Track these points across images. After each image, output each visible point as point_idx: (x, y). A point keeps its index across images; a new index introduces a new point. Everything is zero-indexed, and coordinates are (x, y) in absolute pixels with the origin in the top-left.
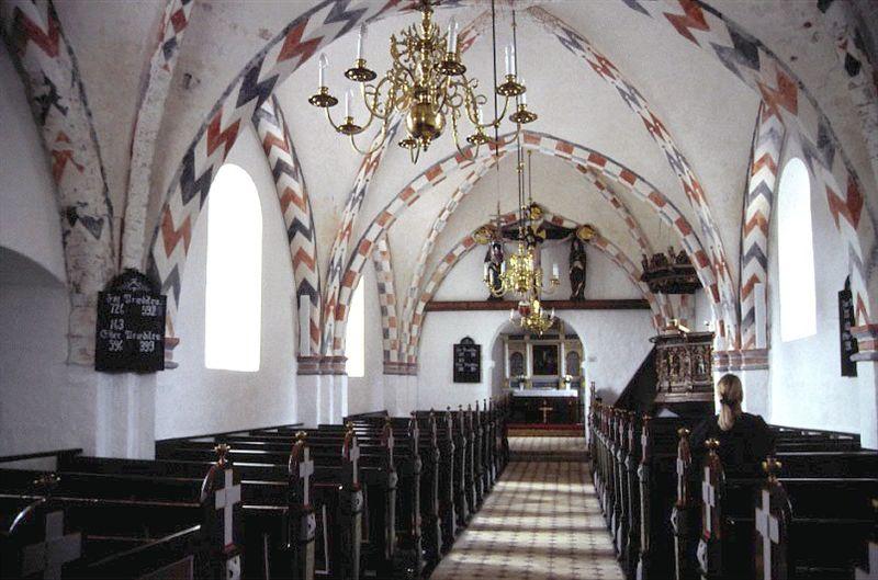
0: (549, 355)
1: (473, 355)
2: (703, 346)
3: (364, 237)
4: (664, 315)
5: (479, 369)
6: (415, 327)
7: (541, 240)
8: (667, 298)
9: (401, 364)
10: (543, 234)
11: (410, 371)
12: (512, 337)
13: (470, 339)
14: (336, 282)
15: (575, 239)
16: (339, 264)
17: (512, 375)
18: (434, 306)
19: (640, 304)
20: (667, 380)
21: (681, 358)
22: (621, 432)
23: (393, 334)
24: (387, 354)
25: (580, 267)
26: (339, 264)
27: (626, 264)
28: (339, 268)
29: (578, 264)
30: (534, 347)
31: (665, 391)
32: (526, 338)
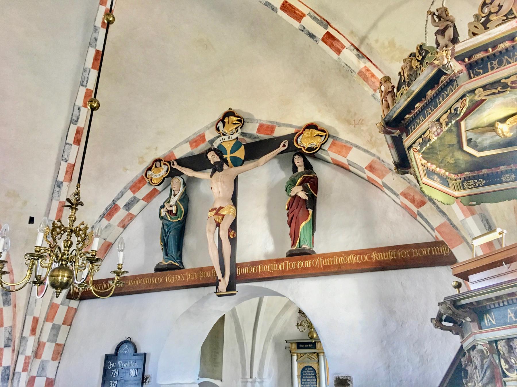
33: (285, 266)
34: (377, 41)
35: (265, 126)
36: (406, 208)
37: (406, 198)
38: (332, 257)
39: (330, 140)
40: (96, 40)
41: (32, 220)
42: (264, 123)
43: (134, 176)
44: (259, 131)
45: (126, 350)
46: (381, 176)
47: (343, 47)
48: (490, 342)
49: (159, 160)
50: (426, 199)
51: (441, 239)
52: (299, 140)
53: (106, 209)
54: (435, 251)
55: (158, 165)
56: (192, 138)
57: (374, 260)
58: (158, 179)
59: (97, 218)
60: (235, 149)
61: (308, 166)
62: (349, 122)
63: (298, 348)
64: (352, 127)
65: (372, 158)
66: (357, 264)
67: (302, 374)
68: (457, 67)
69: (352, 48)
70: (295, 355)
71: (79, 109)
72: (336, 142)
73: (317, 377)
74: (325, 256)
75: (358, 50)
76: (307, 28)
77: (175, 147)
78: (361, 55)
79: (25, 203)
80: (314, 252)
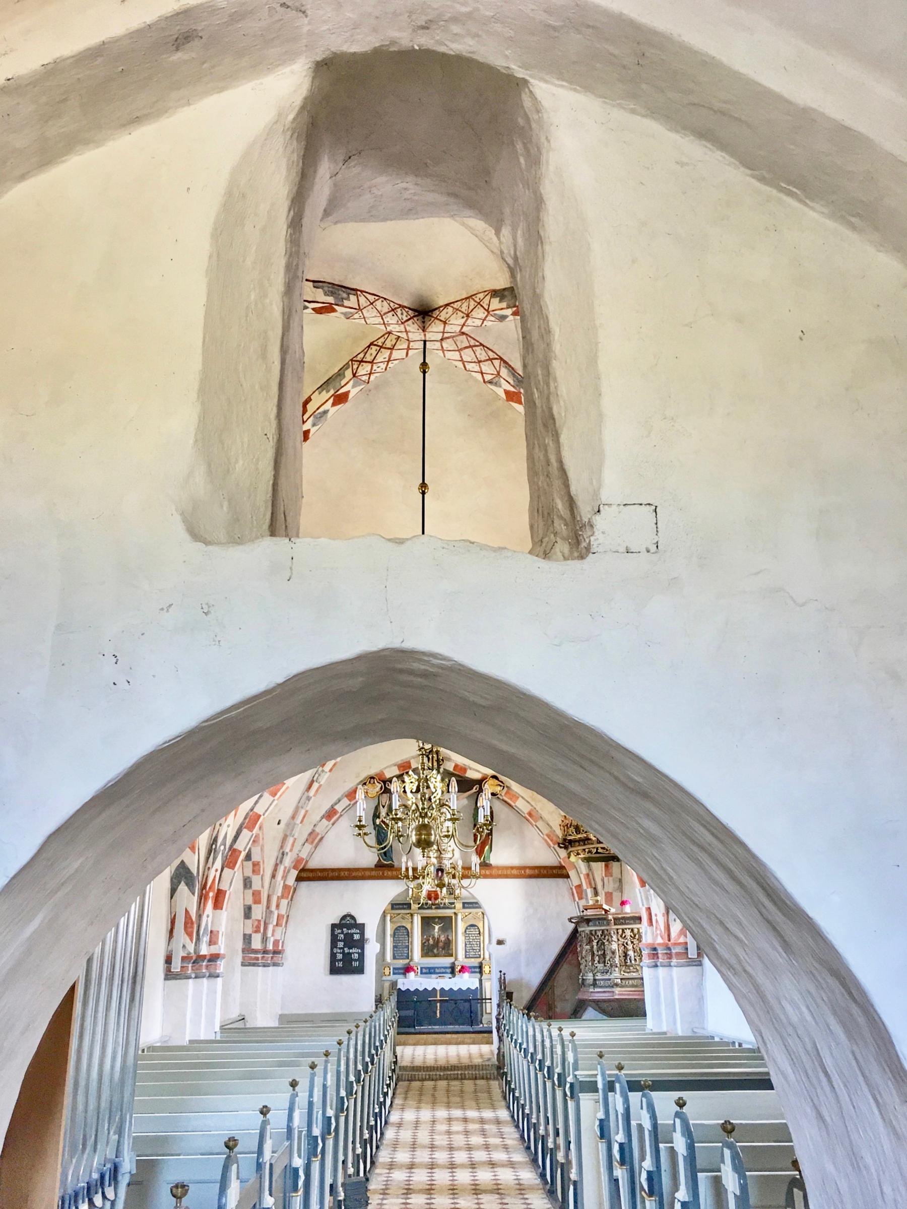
1: (357, 937)
2: (632, 930)
3: (252, 810)
4: (585, 886)
6: (284, 902)
8: (589, 866)
9: (265, 952)
13: (353, 918)
14: (218, 864)
16: (224, 844)
17: (394, 958)
18: (307, 875)
19: (558, 872)
20: (592, 971)
22: (515, 1022)
23: (258, 912)
24: (247, 939)
26: (224, 844)
28: (222, 848)
35: (459, 767)
36: (546, 841)
38: (503, 869)
39: (506, 789)
42: (459, 764)
44: (454, 769)
46: (535, 822)
49: (372, 778)
55: (372, 782)
56: (400, 762)
58: (372, 794)
59: (318, 818)
65: (531, 807)
70: (389, 915)
72: (510, 791)
73: (410, 935)
74: (498, 868)
77: (385, 768)
80: (491, 865)
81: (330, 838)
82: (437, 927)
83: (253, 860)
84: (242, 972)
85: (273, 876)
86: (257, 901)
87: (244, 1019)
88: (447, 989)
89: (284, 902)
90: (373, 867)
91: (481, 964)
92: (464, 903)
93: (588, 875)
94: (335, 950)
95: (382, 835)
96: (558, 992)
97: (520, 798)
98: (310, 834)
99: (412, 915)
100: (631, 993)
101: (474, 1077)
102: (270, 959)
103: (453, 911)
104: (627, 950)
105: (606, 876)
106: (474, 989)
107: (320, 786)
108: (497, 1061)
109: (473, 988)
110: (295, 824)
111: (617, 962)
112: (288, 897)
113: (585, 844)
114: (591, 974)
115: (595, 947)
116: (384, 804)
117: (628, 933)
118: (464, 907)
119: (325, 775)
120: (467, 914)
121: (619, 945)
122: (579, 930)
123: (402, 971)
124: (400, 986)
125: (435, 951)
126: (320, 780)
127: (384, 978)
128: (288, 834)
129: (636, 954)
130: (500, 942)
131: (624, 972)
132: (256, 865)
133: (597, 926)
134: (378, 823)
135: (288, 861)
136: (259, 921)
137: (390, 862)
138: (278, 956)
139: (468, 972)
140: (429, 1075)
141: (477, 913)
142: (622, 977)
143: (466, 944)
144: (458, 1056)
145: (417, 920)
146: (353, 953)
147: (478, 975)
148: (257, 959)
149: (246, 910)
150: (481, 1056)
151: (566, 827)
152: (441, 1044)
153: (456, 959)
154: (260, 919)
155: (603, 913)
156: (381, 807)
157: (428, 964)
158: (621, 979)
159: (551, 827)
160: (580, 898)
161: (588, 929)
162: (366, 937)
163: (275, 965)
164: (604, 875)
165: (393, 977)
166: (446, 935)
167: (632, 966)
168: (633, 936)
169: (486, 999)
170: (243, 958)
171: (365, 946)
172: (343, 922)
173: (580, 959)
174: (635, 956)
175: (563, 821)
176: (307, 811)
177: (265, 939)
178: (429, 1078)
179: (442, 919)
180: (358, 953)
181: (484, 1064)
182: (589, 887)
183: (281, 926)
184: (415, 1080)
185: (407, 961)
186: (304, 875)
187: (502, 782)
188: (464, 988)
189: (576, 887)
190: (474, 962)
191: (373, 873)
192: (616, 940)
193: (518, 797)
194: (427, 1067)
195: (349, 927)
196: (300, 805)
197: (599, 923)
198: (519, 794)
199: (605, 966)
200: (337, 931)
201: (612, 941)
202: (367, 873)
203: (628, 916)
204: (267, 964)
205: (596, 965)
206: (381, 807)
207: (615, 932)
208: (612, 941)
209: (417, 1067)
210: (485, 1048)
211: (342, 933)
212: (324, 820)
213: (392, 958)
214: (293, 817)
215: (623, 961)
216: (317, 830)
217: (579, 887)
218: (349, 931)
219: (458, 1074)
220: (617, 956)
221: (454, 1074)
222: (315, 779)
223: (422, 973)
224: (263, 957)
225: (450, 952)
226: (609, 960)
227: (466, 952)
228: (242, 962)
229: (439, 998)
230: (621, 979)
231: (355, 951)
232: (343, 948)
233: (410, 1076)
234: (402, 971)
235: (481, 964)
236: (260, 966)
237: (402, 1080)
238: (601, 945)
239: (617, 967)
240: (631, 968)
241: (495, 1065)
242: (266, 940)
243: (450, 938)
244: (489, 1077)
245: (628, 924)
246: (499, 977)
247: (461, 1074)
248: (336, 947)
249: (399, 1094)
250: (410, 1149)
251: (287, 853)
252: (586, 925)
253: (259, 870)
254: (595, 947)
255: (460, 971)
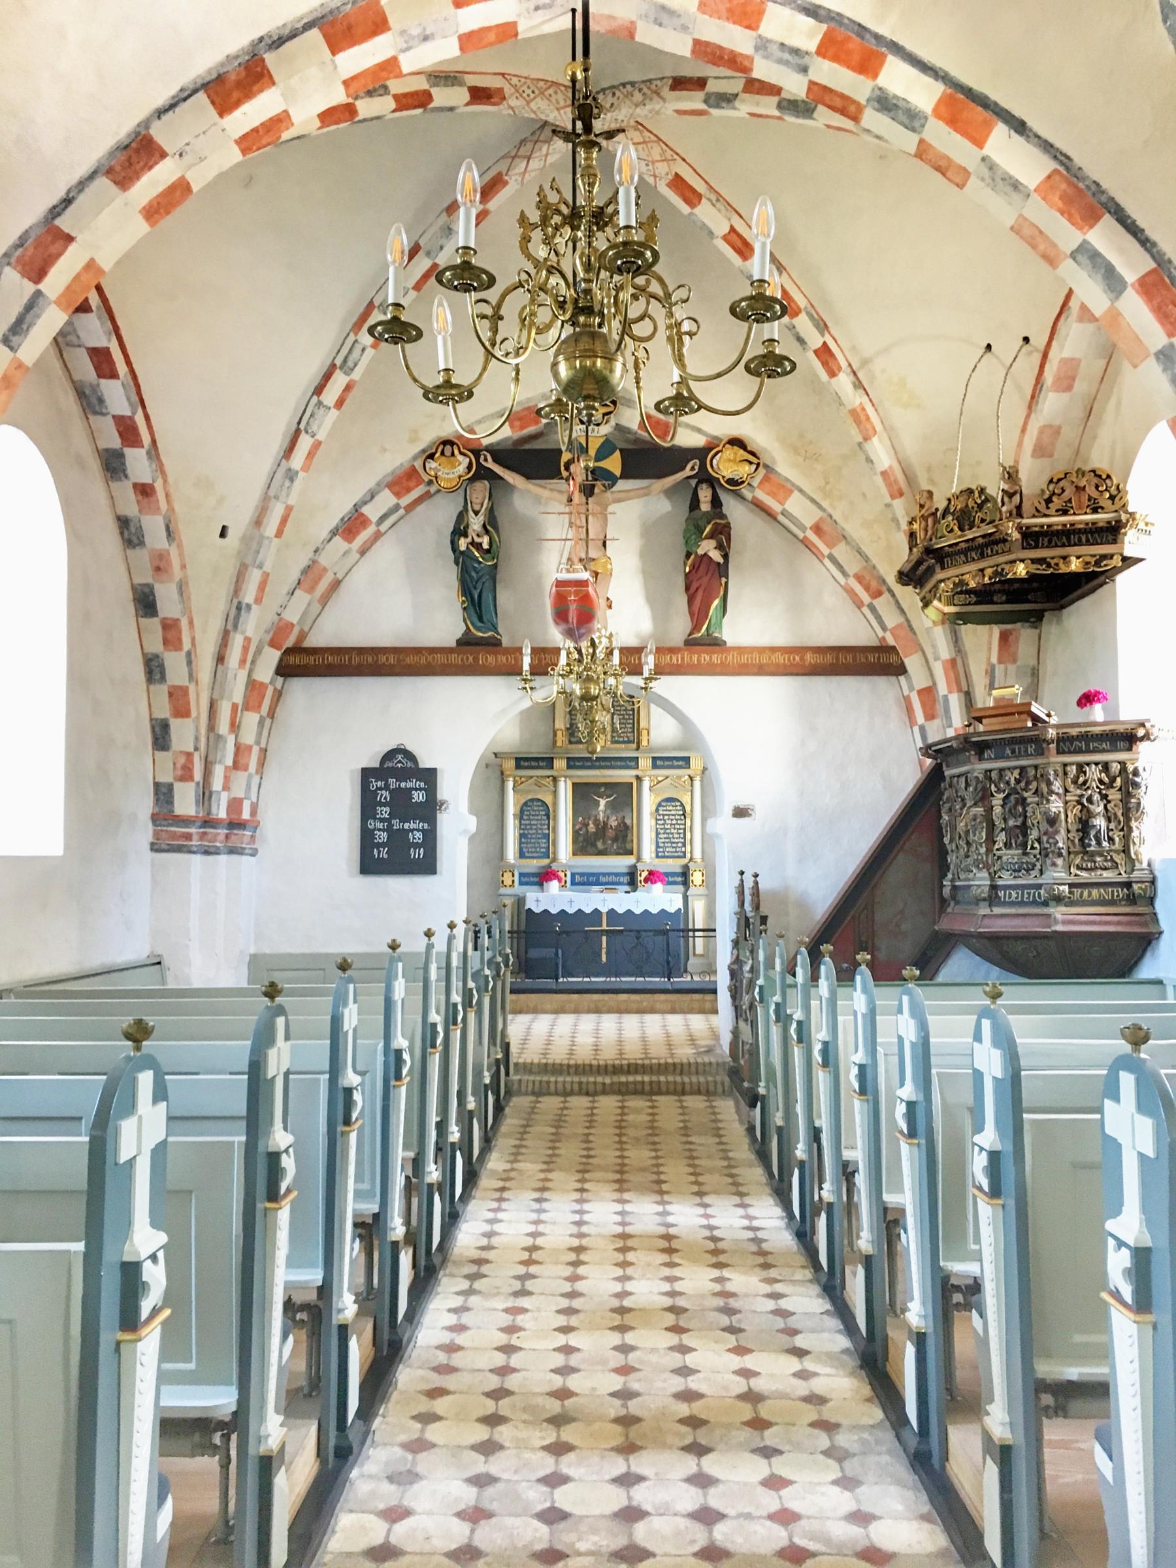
0: (613, 807)
1: (418, 797)
2: (1106, 767)
4: (942, 688)
5: (430, 839)
6: (250, 720)
7: (609, 479)
9: (209, 822)
10: (614, 464)
11: (234, 842)
12: (521, 762)
15: (706, 478)
17: (522, 855)
20: (987, 866)
21: (1031, 799)
23: (183, 734)
24: (163, 793)
25: (716, 556)
27: (841, 551)
29: (708, 547)
30: (575, 786)
31: (978, 901)
32: (560, 764)
33: (683, 658)
34: (883, 371)
37: (860, 582)
38: (752, 653)
39: (762, 472)
40: (442, 248)
41: (223, 533)
43: (397, 464)
44: (642, 425)
45: (400, 762)
46: (830, 545)
47: (840, 369)
48: (986, 771)
50: (884, 588)
51: (891, 641)
52: (715, 462)
53: (342, 519)
54: (884, 659)
57: (807, 663)
58: (449, 480)
59: (324, 534)
60: (603, 453)
61: (716, 502)
62: (795, 450)
63: (518, 766)
64: (801, 459)
66: (784, 665)
67: (522, 811)
68: (1016, 535)
69: (849, 370)
71: (363, 350)
72: (772, 476)
74: (741, 650)
75: (854, 373)
76: (798, 329)
78: (858, 385)
79: (221, 500)
81: (359, 580)
82: (603, 802)
83: (161, 614)
84: (153, 866)
85: (220, 659)
86: (182, 711)
87: (159, 963)
88: (621, 911)
89: (250, 720)
90: (454, 644)
91: (686, 867)
92: (654, 759)
93: (953, 662)
94: (371, 824)
95: (474, 574)
96: (881, 915)
97: (796, 493)
98: (306, 571)
99: (555, 780)
100: (1097, 918)
101: (679, 1088)
102: (222, 837)
103: (634, 772)
104: (1091, 815)
105: (1000, 661)
106: (673, 911)
107: (317, 445)
108: (731, 1055)
109: (672, 910)
110: (262, 537)
111: (1061, 845)
112: (260, 706)
113: (982, 556)
114: (985, 874)
115: (998, 810)
116: (477, 508)
117: (1094, 773)
118: (655, 766)
119: (324, 416)
120: (660, 779)
121: (1066, 803)
122: (948, 773)
123: (536, 880)
124: (530, 904)
125: (600, 845)
126: (314, 428)
127: (503, 891)
128: (248, 561)
129: (1112, 826)
130: (740, 812)
131: (1079, 868)
132: (170, 628)
133: (1008, 758)
134: (463, 548)
135: (254, 625)
136: (189, 756)
137: (490, 634)
138: (241, 832)
139: (661, 881)
140: (580, 1083)
141: (679, 777)
142: (1072, 880)
143: (657, 834)
144: (644, 1039)
145: (565, 791)
146: (412, 831)
147: (681, 888)
148: (188, 837)
149: (157, 729)
150: (692, 1040)
151: (930, 521)
152: (609, 1011)
153: (639, 859)
154: (192, 750)
155: (1030, 724)
156: (471, 513)
157: (583, 866)
158: (1071, 885)
159: (867, 559)
160: (930, 716)
161: (978, 768)
162: (439, 797)
163: (232, 851)
164: (994, 660)
165: (518, 889)
166: (620, 815)
167: (1101, 855)
168: (1106, 780)
169: (694, 930)
170: (156, 834)
171: (439, 816)
172: (389, 764)
173: (946, 840)
174: (1109, 830)
175: (922, 506)
176: (289, 509)
177: (205, 795)
178: (580, 1089)
179: (611, 787)
180: (423, 831)
181: (699, 1060)
182: (955, 688)
183: (246, 769)
184: (549, 1094)
185: (546, 862)
186: (293, 660)
187: (753, 454)
188: (654, 911)
189: (920, 692)
190: (672, 865)
191: (454, 659)
192: (1061, 791)
193: (791, 492)
194: (577, 1066)
195: (403, 774)
196: (272, 493)
197: (1013, 752)
198: (793, 485)
199: (1025, 854)
200: (376, 784)
201: (1051, 792)
202: (440, 659)
203: (1097, 730)
204: (212, 850)
205: (998, 853)
206: (471, 513)
207: (1060, 770)
208: (1051, 792)
209: (554, 1064)
210: (698, 1022)
211: (387, 787)
212: (337, 539)
213: (517, 855)
214: (258, 522)
215: (1076, 841)
216: (323, 560)
217: (928, 694)
218: (403, 785)
219: (643, 1083)
220: (1063, 832)
221: (635, 1083)
222: (302, 426)
223: (573, 883)
224: (205, 833)
225: (628, 846)
226: (1039, 840)
227: (658, 846)
228: (152, 844)
229: (605, 927)
230: (1071, 885)
231: (416, 826)
232: (388, 820)
233: (537, 1084)
234: (536, 880)
235: (686, 867)
236: (194, 852)
237: (519, 1093)
238: (1016, 802)
239: (1060, 855)
240: (1098, 859)
241: (724, 1063)
242: (210, 797)
243: (628, 822)
244: (711, 1088)
245: (1096, 751)
246: (737, 883)
247: (651, 1083)
248: (375, 818)
249: (506, 1136)
250: (567, 1118)
251: (249, 607)
252: (974, 759)
253: (180, 640)
254: (998, 810)
255: (646, 880)
